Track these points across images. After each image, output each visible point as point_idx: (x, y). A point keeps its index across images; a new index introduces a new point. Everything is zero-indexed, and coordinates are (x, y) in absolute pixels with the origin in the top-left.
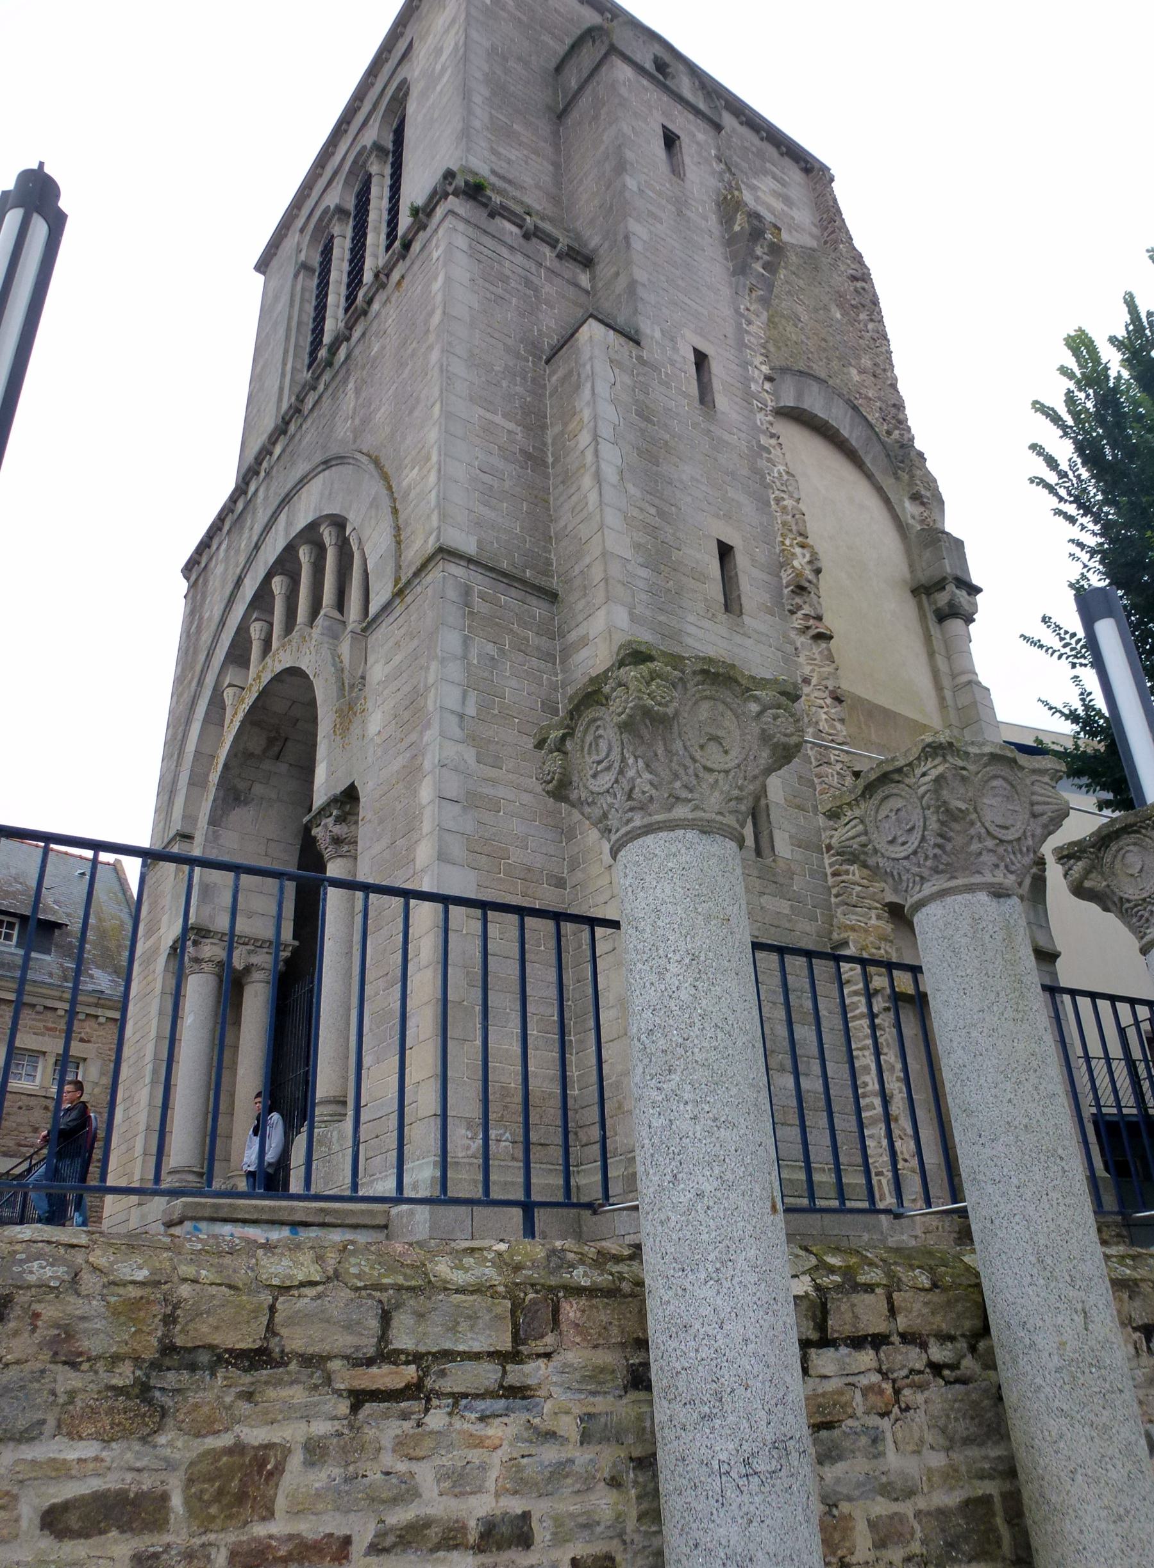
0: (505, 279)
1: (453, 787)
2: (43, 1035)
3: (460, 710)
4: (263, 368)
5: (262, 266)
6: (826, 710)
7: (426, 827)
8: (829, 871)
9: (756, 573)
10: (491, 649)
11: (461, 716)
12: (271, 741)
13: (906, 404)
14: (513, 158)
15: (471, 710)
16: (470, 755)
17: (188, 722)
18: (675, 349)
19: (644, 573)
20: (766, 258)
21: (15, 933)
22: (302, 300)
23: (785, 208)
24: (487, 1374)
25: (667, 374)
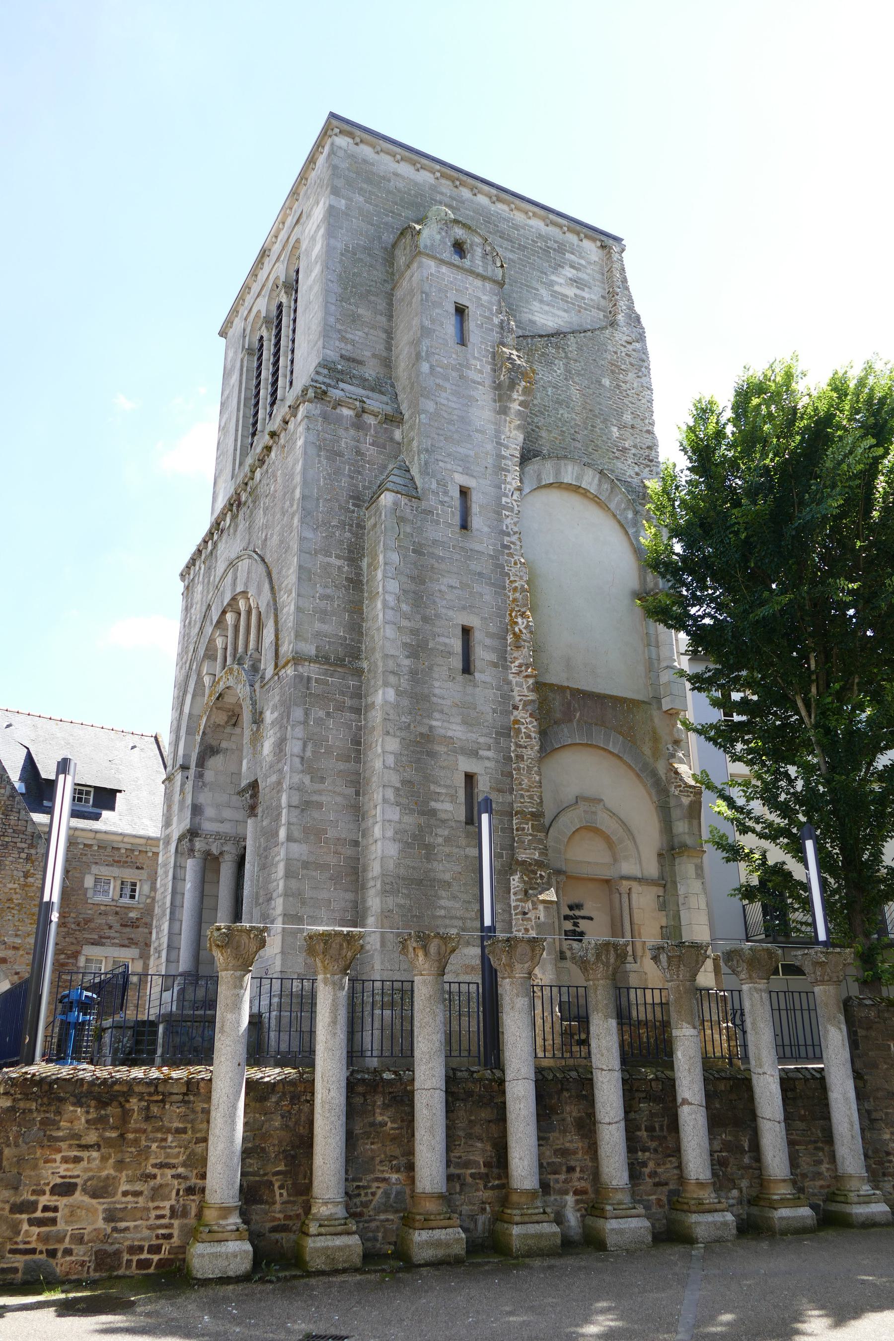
1: (295, 801)
2: (112, 865)
3: (301, 754)
5: (223, 333)
7: (284, 820)
8: (515, 827)
9: (488, 641)
11: (302, 758)
12: (230, 718)
13: (660, 444)
15: (309, 754)
16: (307, 780)
17: (185, 693)
18: (446, 493)
19: (407, 662)
20: (521, 398)
23: (578, 292)
25: (437, 514)
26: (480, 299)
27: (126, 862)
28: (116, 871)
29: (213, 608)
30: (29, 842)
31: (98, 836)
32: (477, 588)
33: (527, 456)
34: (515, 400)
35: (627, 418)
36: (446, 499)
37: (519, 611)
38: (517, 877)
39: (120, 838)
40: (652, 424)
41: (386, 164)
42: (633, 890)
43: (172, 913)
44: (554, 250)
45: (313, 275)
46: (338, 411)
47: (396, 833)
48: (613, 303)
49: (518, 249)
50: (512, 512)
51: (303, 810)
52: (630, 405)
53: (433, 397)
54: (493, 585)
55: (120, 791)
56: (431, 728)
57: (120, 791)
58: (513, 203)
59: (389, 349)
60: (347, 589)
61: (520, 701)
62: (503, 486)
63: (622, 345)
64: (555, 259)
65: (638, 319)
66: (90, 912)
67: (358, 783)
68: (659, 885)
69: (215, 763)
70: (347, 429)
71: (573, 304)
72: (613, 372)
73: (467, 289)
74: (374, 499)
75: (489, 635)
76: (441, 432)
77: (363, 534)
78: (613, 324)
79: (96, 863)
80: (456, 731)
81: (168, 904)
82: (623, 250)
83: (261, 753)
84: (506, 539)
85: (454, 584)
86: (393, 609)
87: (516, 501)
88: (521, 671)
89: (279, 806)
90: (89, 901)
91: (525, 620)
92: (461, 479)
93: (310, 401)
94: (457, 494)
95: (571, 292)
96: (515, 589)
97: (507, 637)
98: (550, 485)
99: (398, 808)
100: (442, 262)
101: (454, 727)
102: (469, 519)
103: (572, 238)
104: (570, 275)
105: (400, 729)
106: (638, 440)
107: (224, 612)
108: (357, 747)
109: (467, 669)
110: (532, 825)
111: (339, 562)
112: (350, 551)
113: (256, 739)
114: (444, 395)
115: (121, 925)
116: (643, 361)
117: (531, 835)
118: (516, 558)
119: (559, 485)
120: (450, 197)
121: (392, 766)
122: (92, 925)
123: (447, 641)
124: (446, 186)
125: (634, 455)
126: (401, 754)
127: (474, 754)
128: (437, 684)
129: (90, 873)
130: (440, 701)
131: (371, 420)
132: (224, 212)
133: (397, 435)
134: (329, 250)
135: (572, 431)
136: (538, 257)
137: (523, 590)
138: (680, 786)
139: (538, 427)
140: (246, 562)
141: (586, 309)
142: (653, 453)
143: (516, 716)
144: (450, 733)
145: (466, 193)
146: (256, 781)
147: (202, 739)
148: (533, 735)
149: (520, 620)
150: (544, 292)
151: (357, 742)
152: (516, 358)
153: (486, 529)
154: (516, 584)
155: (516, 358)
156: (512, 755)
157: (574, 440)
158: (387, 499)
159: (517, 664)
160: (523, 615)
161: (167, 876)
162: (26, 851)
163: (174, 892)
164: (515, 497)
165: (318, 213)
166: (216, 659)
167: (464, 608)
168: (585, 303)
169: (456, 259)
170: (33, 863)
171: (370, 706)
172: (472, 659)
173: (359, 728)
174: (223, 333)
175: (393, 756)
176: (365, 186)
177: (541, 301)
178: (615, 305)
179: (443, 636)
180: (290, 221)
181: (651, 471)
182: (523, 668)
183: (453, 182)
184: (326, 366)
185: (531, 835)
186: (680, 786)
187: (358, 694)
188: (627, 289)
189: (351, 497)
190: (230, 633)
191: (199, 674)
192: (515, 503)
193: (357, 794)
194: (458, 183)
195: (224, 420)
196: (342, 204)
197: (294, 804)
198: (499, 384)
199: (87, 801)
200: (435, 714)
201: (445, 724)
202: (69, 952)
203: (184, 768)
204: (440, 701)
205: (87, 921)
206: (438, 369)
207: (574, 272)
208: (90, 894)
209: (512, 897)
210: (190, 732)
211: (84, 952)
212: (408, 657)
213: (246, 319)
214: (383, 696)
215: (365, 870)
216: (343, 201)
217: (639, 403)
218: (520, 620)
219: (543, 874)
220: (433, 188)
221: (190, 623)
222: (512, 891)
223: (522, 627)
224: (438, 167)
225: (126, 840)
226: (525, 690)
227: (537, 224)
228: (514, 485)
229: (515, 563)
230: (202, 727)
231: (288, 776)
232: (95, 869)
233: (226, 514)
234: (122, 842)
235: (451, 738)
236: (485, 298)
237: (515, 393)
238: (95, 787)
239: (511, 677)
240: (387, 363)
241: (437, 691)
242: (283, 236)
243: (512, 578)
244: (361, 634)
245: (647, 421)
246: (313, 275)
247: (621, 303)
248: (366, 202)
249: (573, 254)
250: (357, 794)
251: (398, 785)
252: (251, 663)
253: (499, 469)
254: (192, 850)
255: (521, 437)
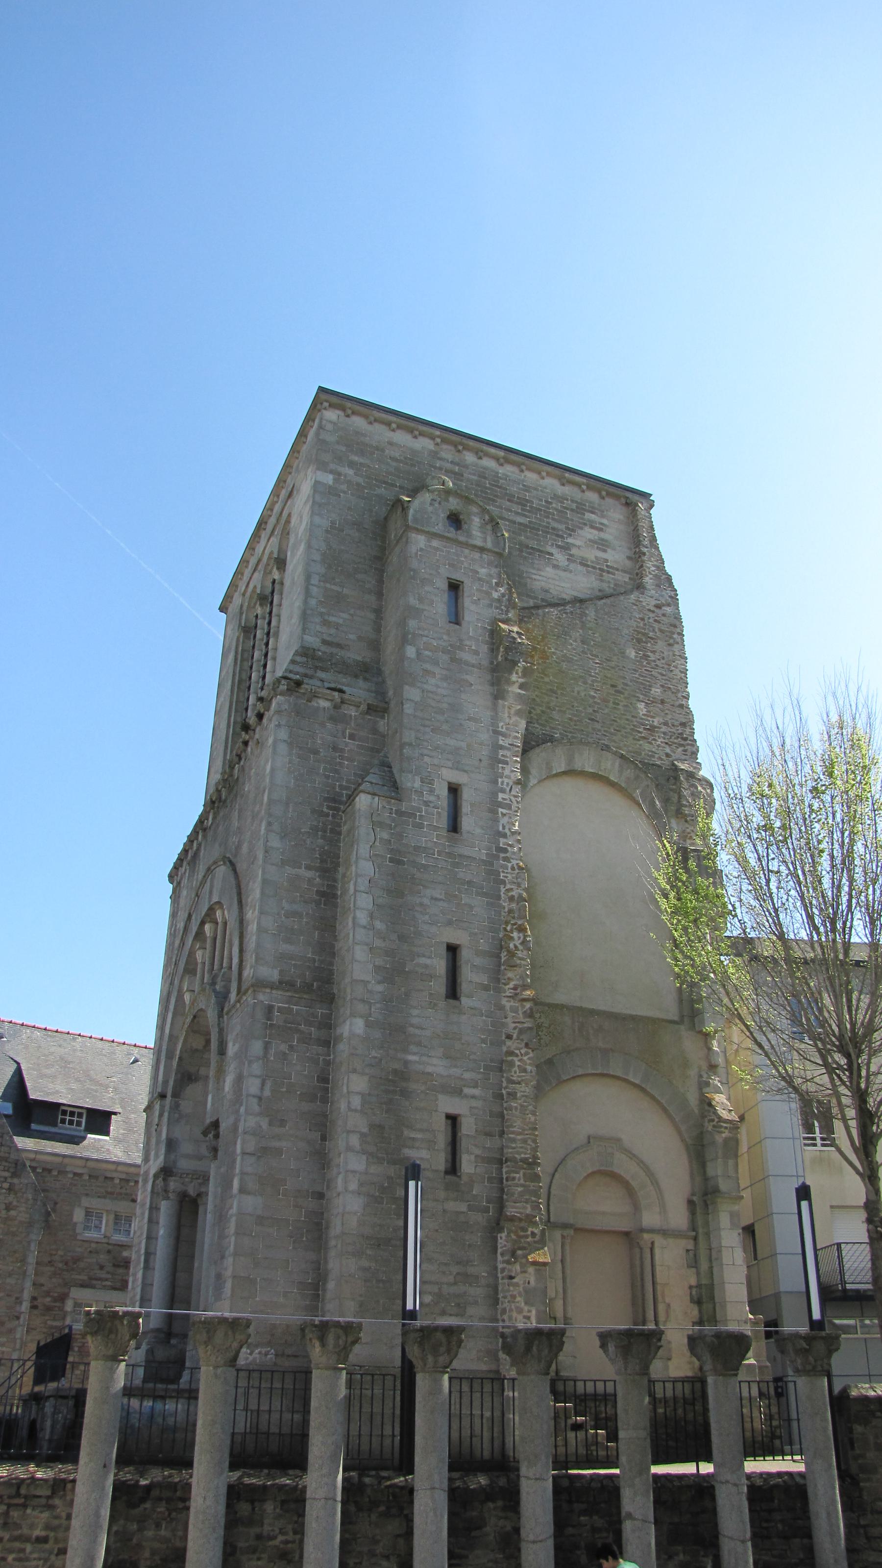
0: (316, 752)
1: (251, 1147)
2: (105, 1197)
3: (259, 1094)
4: (221, 706)
5: (222, 609)
6: (520, 1057)
8: (505, 1176)
9: (478, 961)
10: (284, 1047)
11: (260, 1098)
14: (341, 621)
15: (267, 1093)
18: (432, 791)
19: (380, 988)
20: (521, 680)
21: (84, 1121)
22: (242, 660)
23: (601, 554)
24: (43, 1501)
26: (477, 572)
27: (121, 1194)
28: (108, 1204)
29: (193, 917)
30: (12, 1170)
31: (89, 1164)
32: (465, 899)
33: (529, 745)
34: (514, 683)
35: (656, 691)
36: (432, 798)
37: (515, 924)
38: (504, 1235)
39: (112, 1167)
40: (687, 698)
41: (380, 434)
42: (656, 1244)
43: (147, 1261)
44: (572, 510)
45: (299, 553)
46: (314, 704)
47: (361, 1185)
48: (640, 564)
49: (529, 511)
50: (510, 808)
51: (259, 1157)
52: (660, 677)
53: (419, 684)
54: (485, 895)
55: (115, 1114)
56: (406, 1063)
57: (115, 1114)
58: (523, 464)
59: (378, 629)
60: (318, 903)
61: (515, 1028)
62: (500, 780)
63: (649, 610)
64: (572, 520)
65: (669, 579)
66: (79, 1250)
67: (322, 1126)
68: (686, 1237)
69: (192, 1090)
70: (323, 725)
71: (594, 568)
72: (639, 641)
73: (462, 562)
74: (351, 798)
75: (479, 953)
76: (427, 723)
77: (338, 841)
78: (640, 587)
79: (87, 1195)
80: (437, 1065)
81: (143, 1251)
82: (652, 506)
83: (223, 1089)
84: (502, 840)
85: (438, 896)
86: (365, 927)
87: (515, 796)
88: (516, 994)
89: (234, 1152)
90: (79, 1237)
91: (521, 935)
92: (451, 775)
93: (282, 694)
94: (444, 792)
95: (592, 554)
96: (511, 899)
97: (500, 957)
98: (564, 773)
99: (364, 1157)
100: (435, 535)
101: (435, 1061)
102: (459, 819)
103: (593, 496)
104: (589, 536)
105: (371, 1065)
106: (670, 717)
107: (203, 923)
108: (323, 1085)
109: (453, 992)
110: (524, 1174)
111: (309, 874)
112: (322, 861)
113: (221, 1072)
114: (432, 681)
115: (114, 1265)
116: (675, 626)
117: (522, 1185)
118: (514, 862)
119: (570, 773)
120: (452, 462)
121: (359, 1108)
122: (82, 1265)
123: (428, 961)
124: (447, 453)
125: (664, 733)
126: (369, 1094)
127: (457, 1092)
128: (415, 1012)
129: (79, 1206)
130: (417, 1031)
131: (353, 712)
132: (234, 476)
133: (382, 725)
134: (312, 526)
135: (590, 710)
136: (553, 519)
137: (521, 898)
138: (713, 1120)
139: (549, 708)
140: (223, 868)
141: (608, 572)
142: (688, 730)
143: (509, 1047)
144: (429, 1069)
145: (470, 458)
146: (218, 1120)
147: (179, 1065)
148: (529, 1068)
149: (515, 935)
150: (560, 557)
151: (324, 1079)
152: (516, 636)
153: (478, 831)
154: (513, 893)
155: (516, 636)
156: (504, 1092)
157: (592, 720)
158: (363, 801)
159: (511, 985)
160: (521, 929)
161: (143, 1218)
162: (9, 1180)
163: (149, 1238)
164: (513, 793)
165: (305, 489)
166: (195, 975)
167: (450, 923)
168: (607, 566)
169: (452, 533)
170: (16, 1194)
171: (339, 1039)
172: (458, 981)
173: (328, 1063)
174: (222, 609)
175: (360, 1096)
176: (356, 458)
177: (555, 567)
178: (642, 566)
179: (424, 956)
180: (284, 493)
181: (685, 751)
182: (518, 991)
183: (456, 446)
184: (306, 653)
185: (522, 1185)
186: (713, 1120)
187: (328, 1024)
188: (657, 548)
189: (326, 799)
190: (208, 945)
191: (180, 991)
192: (513, 799)
193: (324, 1138)
194: (460, 448)
195: (219, 703)
196: (329, 479)
197: (248, 1151)
198: (497, 665)
199: (79, 1124)
200: (411, 1047)
201: (424, 1059)
202: (56, 1295)
203: (163, 1096)
204: (417, 1031)
205: (76, 1260)
206: (427, 653)
207: (595, 532)
208: (79, 1229)
209: (499, 1258)
210: (170, 1056)
211: (71, 1295)
212: (379, 983)
213: (244, 595)
214: (353, 1027)
215: (327, 1228)
216: (331, 477)
217: (671, 675)
218: (515, 935)
219: (536, 1231)
220: (434, 455)
221: (175, 930)
222: (499, 1251)
223: (517, 943)
224: (438, 433)
225: (120, 1168)
226: (521, 1015)
227: (551, 483)
228: (513, 778)
229: (513, 869)
230: (178, 1052)
231: (243, 1118)
232: (86, 1202)
233: (209, 812)
234: (116, 1171)
235: (429, 1073)
236: (483, 571)
237: (514, 675)
238: (87, 1109)
239: (504, 1001)
240: (375, 646)
241: (415, 1021)
242: (277, 508)
243: (508, 886)
244: (333, 955)
245: (680, 695)
246: (299, 553)
247: (649, 564)
248: (355, 474)
249: (593, 513)
250: (324, 1138)
251: (365, 1130)
252: (223, 983)
253: (495, 761)
254: (166, 1191)
255: (523, 724)
